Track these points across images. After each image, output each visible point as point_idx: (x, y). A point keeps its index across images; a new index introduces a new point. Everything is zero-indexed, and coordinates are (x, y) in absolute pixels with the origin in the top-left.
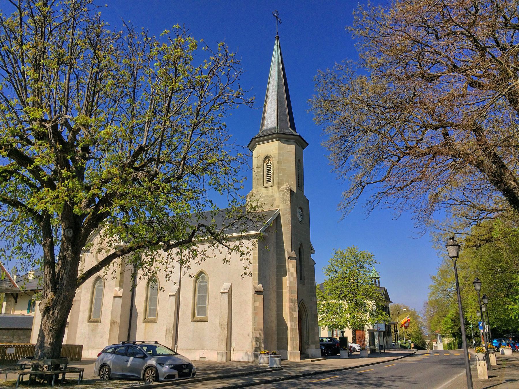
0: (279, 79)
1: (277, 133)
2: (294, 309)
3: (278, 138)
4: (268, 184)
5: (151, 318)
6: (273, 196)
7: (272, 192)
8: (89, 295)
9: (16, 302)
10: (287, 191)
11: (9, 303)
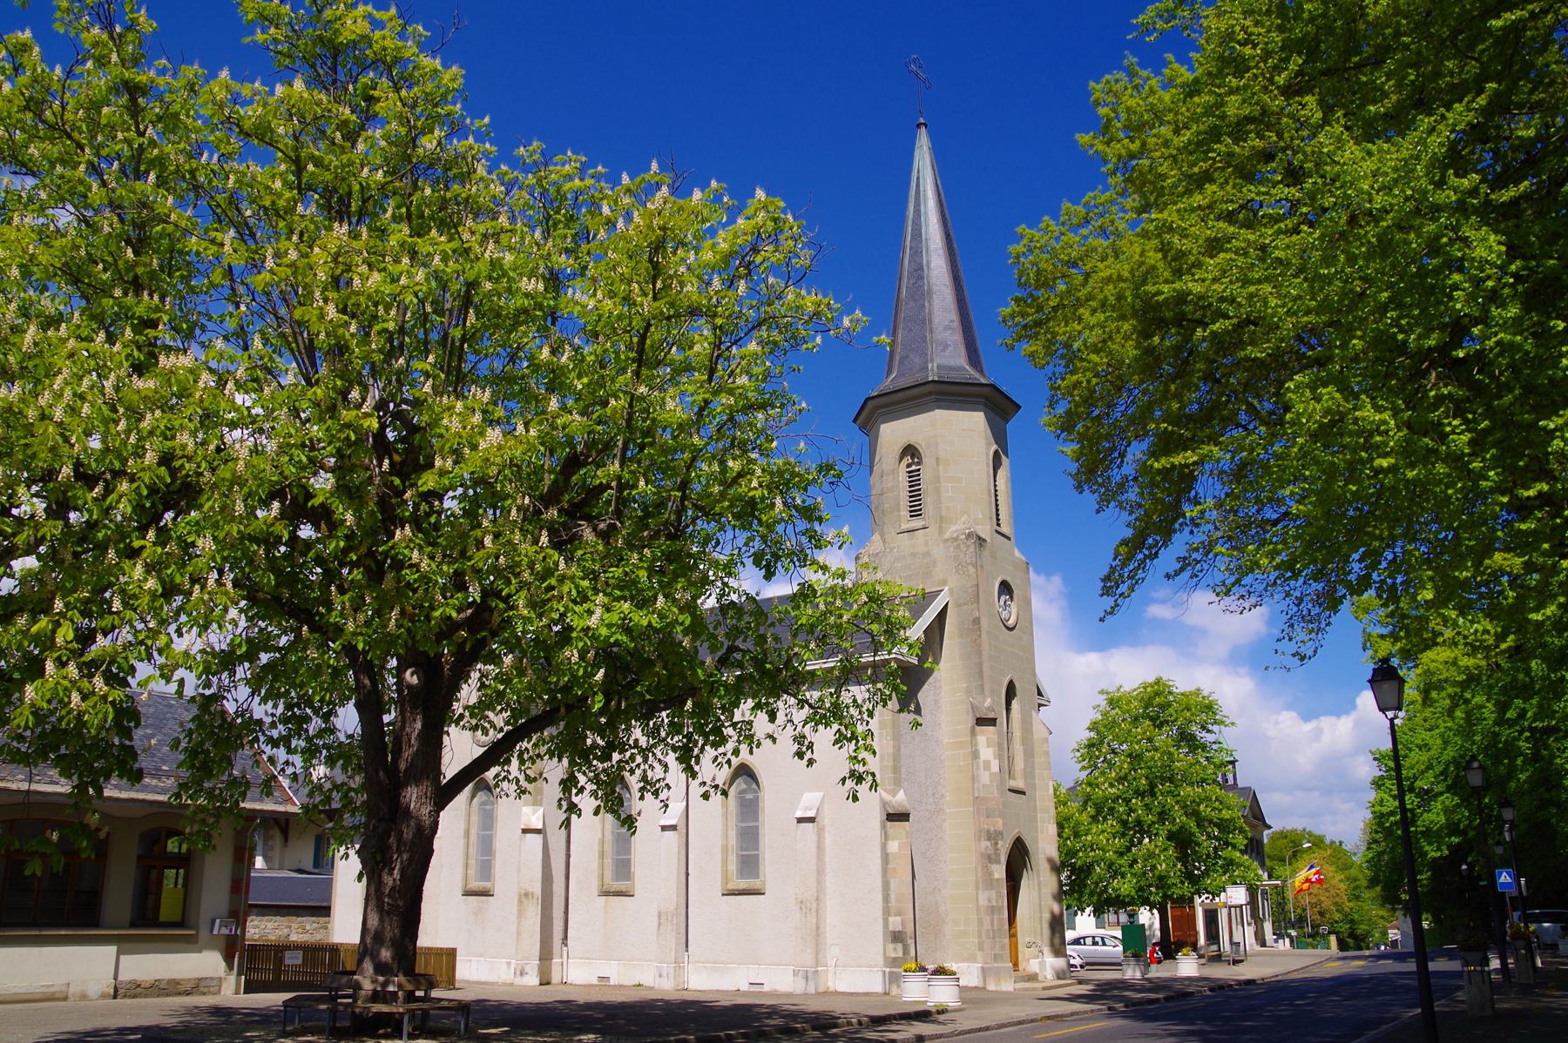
0: (936, 198)
1: (933, 382)
2: (993, 857)
3: (937, 393)
4: (917, 523)
5: (620, 885)
6: (927, 554)
7: (927, 544)
8: (461, 826)
9: (286, 840)
10: (967, 539)
11: (270, 843)
